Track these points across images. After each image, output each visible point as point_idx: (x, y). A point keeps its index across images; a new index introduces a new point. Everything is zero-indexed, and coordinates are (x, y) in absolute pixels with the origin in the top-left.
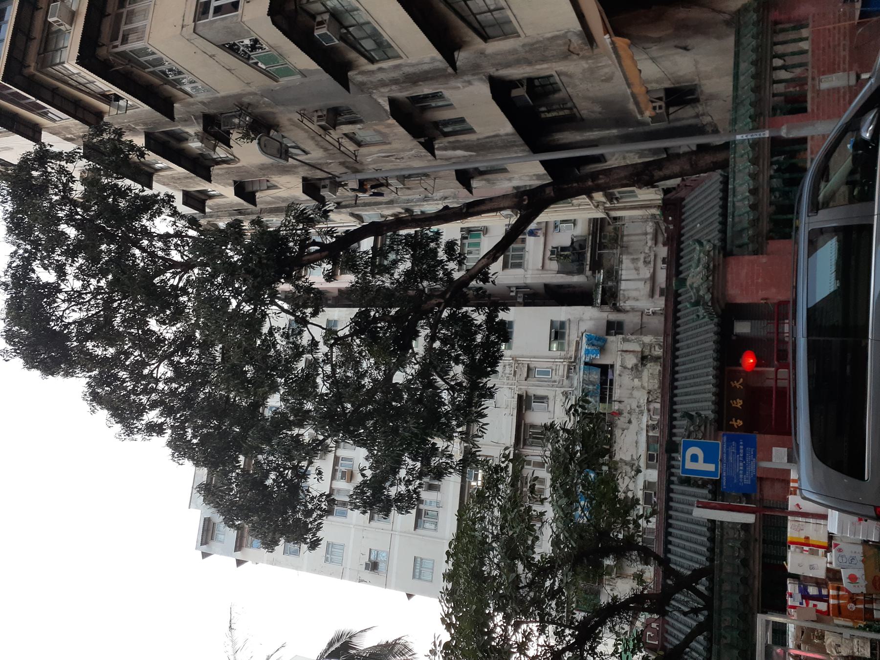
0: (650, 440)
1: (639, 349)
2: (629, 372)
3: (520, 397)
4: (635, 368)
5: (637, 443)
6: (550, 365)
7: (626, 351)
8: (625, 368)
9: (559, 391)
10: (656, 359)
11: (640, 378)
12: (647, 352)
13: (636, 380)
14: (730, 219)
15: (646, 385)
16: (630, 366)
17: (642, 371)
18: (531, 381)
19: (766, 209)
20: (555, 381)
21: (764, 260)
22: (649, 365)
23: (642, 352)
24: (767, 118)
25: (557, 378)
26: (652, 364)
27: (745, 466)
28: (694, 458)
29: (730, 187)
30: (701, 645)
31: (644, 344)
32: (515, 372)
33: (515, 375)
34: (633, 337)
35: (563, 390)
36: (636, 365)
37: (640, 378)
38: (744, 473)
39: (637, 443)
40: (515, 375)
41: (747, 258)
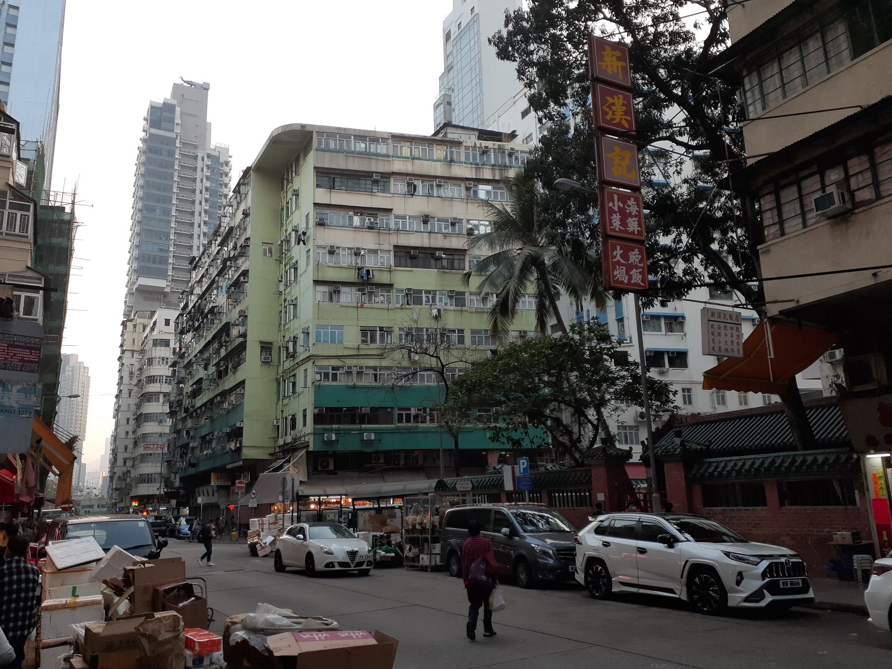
28: (523, 464)
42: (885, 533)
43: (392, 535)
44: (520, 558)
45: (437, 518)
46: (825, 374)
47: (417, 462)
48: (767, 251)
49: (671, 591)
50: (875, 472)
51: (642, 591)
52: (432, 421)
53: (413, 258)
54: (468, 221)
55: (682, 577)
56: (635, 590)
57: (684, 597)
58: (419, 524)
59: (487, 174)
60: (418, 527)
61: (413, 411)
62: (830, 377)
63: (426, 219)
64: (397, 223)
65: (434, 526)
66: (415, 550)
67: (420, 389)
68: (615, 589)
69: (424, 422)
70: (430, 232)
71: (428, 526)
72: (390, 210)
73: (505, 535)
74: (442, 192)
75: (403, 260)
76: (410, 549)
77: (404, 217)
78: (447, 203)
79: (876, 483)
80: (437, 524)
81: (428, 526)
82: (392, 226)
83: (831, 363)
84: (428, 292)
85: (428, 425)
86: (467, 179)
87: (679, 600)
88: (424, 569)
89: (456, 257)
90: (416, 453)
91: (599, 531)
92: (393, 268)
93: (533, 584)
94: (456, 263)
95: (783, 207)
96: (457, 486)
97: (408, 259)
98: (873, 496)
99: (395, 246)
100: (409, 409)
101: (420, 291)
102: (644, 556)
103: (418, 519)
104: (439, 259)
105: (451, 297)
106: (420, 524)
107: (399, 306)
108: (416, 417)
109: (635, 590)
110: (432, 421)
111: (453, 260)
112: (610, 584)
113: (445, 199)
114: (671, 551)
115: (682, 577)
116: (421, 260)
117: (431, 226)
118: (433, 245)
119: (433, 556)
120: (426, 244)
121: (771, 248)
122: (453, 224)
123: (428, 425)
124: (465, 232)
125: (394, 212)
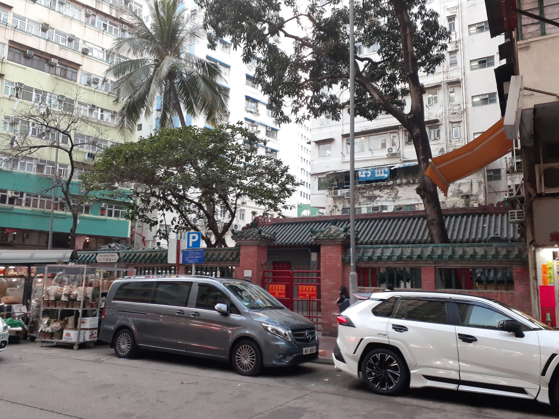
0: (413, 207)
1: (474, 192)
2: (457, 188)
3: (437, 121)
4: (460, 192)
5: (410, 199)
6: (463, 136)
7: (472, 185)
8: (459, 186)
9: (444, 146)
10: (467, 204)
11: (453, 196)
12: (471, 198)
13: (451, 194)
14: (369, 246)
15: (449, 200)
16: (461, 188)
17: (458, 197)
18: (449, 126)
19: (400, 266)
20: (451, 142)
21: (338, 265)
22: (463, 200)
23: (472, 195)
24: (433, 265)
25: (453, 142)
26: (464, 202)
27: (191, 259)
28: (194, 238)
29: (390, 245)
30: (394, 238)
31: (478, 195)
32: (455, 113)
33: (453, 114)
34: (482, 188)
35: (445, 148)
36: (462, 192)
37: (453, 196)
38: (190, 259)
39: (410, 199)
40: (453, 114)
41: (340, 256)
42: (548, 315)
43: (14, 306)
44: (244, 340)
45: (90, 290)
46: (328, 204)
47: (7, 239)
48: (527, 47)
49: (521, 390)
50: (545, 263)
51: (463, 388)
52: (27, 204)
53: (27, 57)
54: (84, 42)
55: (543, 373)
56: (453, 387)
57: (544, 398)
58: (65, 295)
59: (105, 9)
60: (64, 298)
61: (9, 194)
62: (331, 207)
63: (45, 28)
64: (14, 21)
65: (86, 298)
66: (56, 325)
67: (20, 175)
68: (415, 383)
69: (20, 204)
70: (48, 40)
71: (80, 298)
72: (10, 8)
73: (220, 311)
74: (63, 9)
75: (17, 56)
76: (48, 324)
77: (23, 19)
78: (67, 20)
79: (545, 272)
80: (90, 296)
81: (80, 298)
82: (10, 22)
83: (334, 198)
84: (37, 91)
85: (23, 208)
86: (88, 7)
87: (535, 401)
88: (69, 346)
89: (69, 68)
90: (7, 230)
91: (382, 310)
92: (6, 60)
93: (262, 370)
94: (69, 74)
95: (545, 9)
96: (98, 258)
97: (22, 57)
98: (540, 283)
99: (11, 42)
100: (6, 191)
101: (31, 89)
102: (471, 345)
103: (65, 289)
104: (52, 66)
105: (60, 101)
106: (68, 295)
107: (8, 96)
108: (12, 200)
109: (453, 387)
110: (27, 204)
111: (66, 70)
112: (407, 376)
113: (66, 16)
114: (519, 340)
115: (543, 373)
116: (35, 62)
117: (49, 35)
118: (49, 52)
119: (82, 332)
120: (42, 49)
121: (532, 45)
122: (70, 40)
123: (23, 208)
124: (80, 50)
125: (13, 10)
